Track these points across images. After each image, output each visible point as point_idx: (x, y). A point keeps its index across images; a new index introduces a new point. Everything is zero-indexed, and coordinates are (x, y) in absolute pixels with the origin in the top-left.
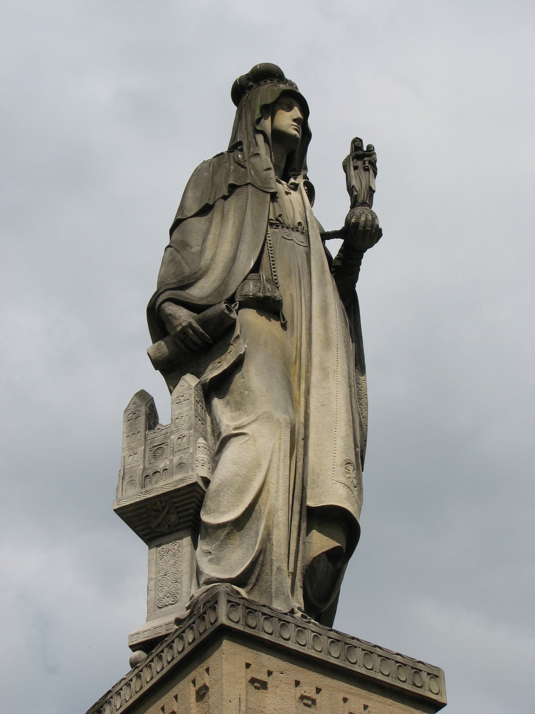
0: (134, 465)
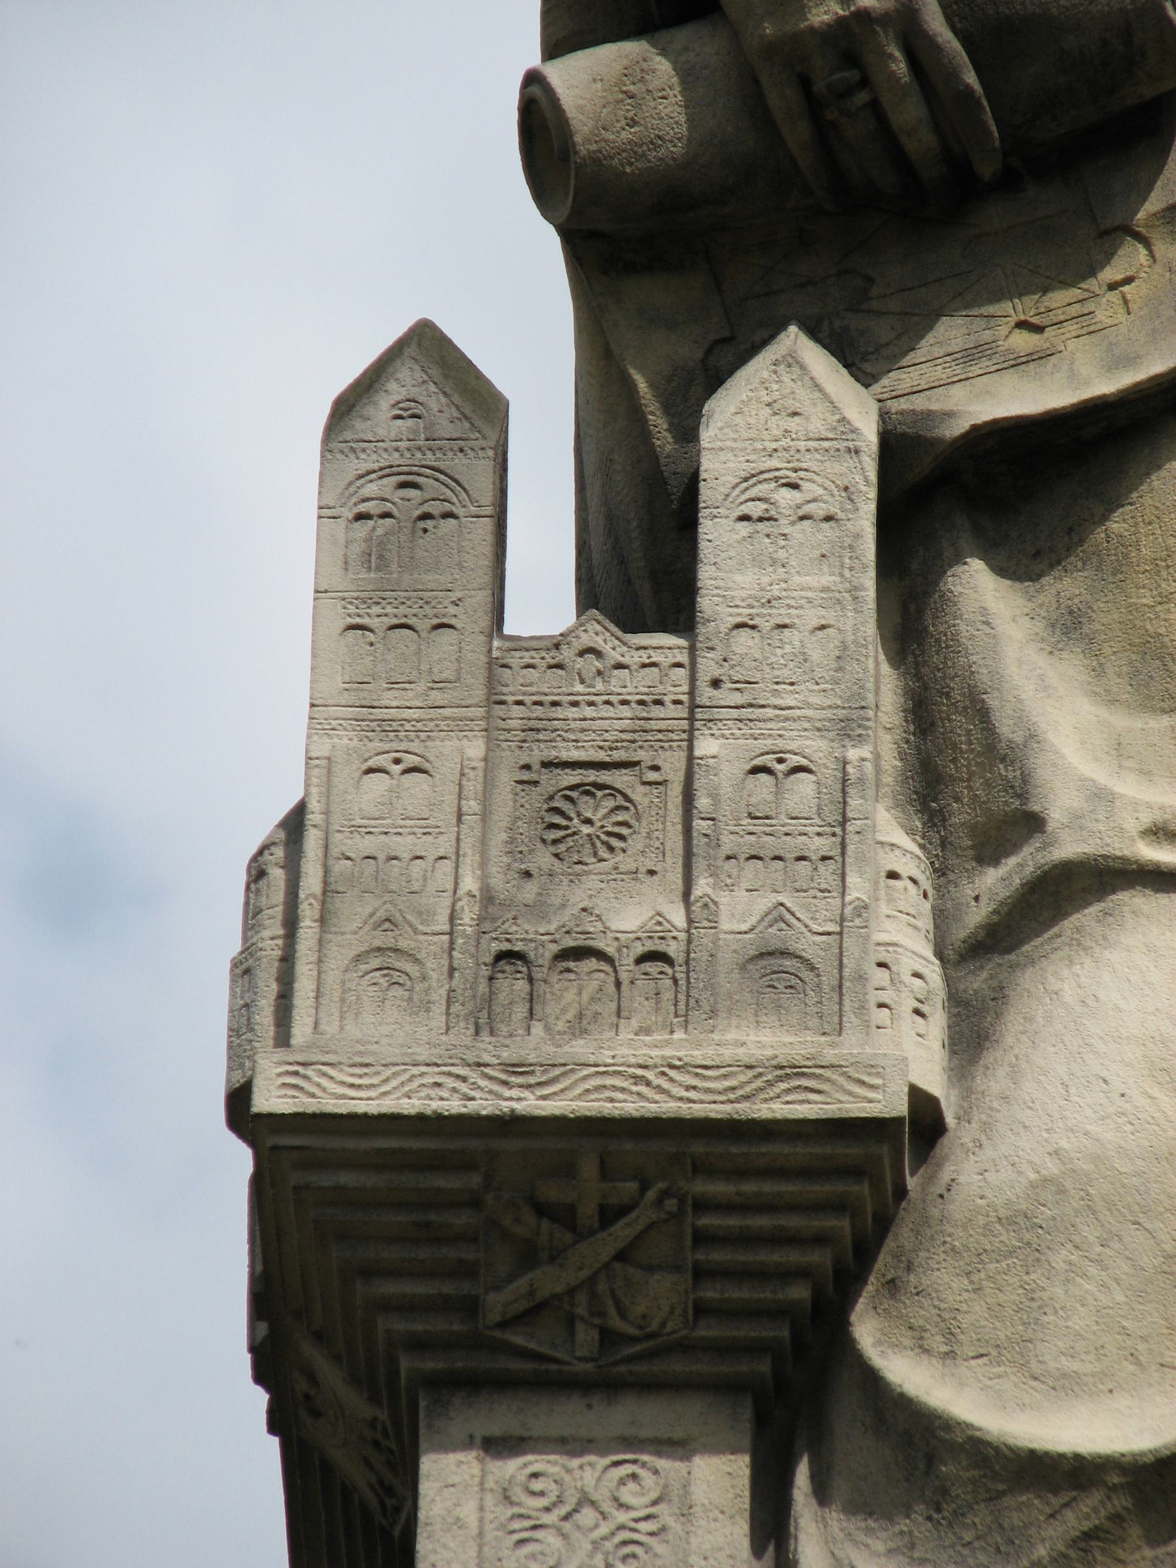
0: (404, 845)
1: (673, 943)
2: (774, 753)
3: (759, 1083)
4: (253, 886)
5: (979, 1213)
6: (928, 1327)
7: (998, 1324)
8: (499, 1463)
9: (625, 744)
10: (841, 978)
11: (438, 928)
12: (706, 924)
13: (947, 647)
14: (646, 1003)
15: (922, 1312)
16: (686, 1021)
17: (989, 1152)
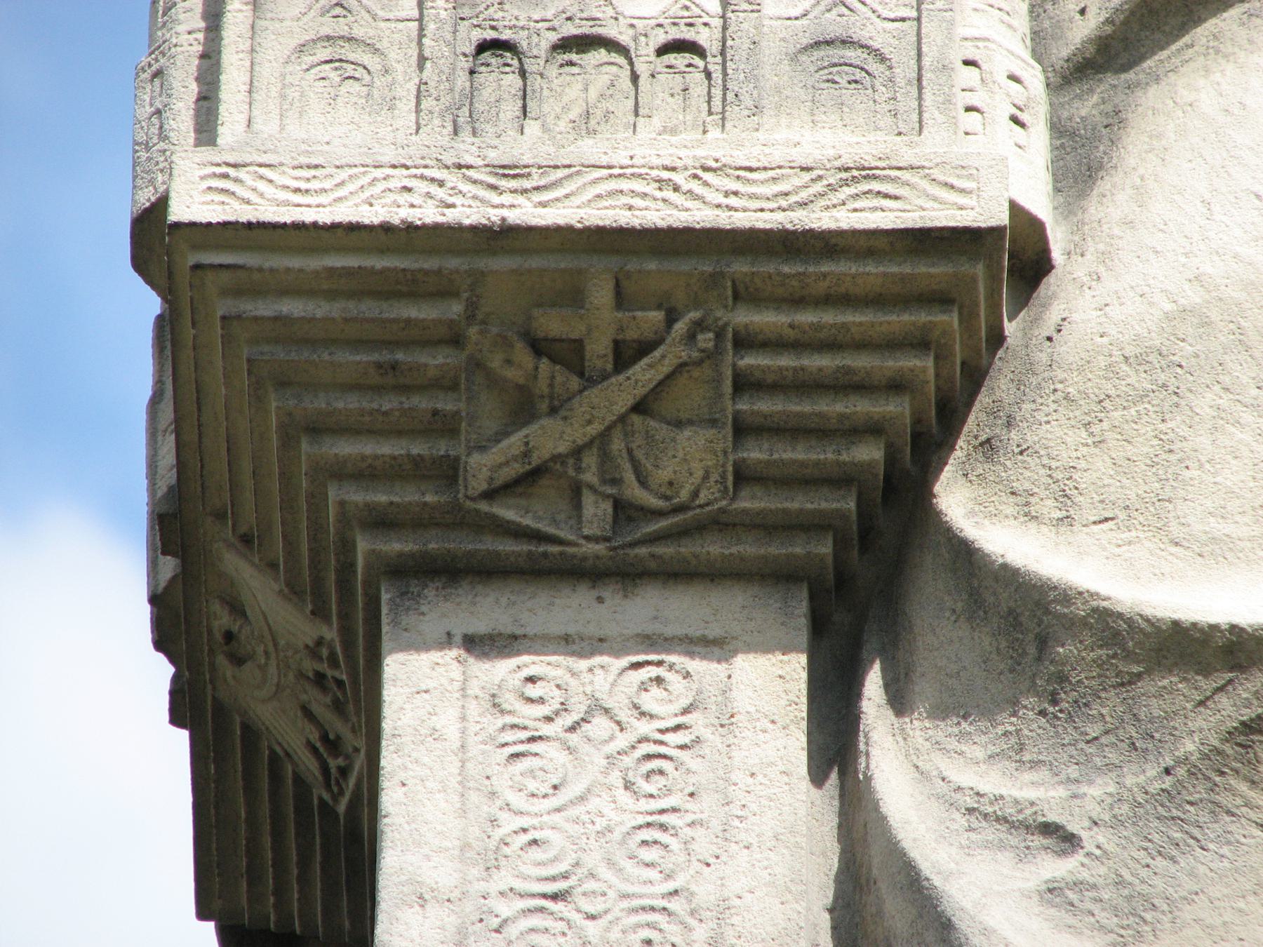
1: (705, 32)
3: (818, 187)
6: (1036, 490)
8: (486, 665)
10: (920, 69)
11: (403, 14)
12: (745, 6)
14: (670, 100)
16: (723, 119)
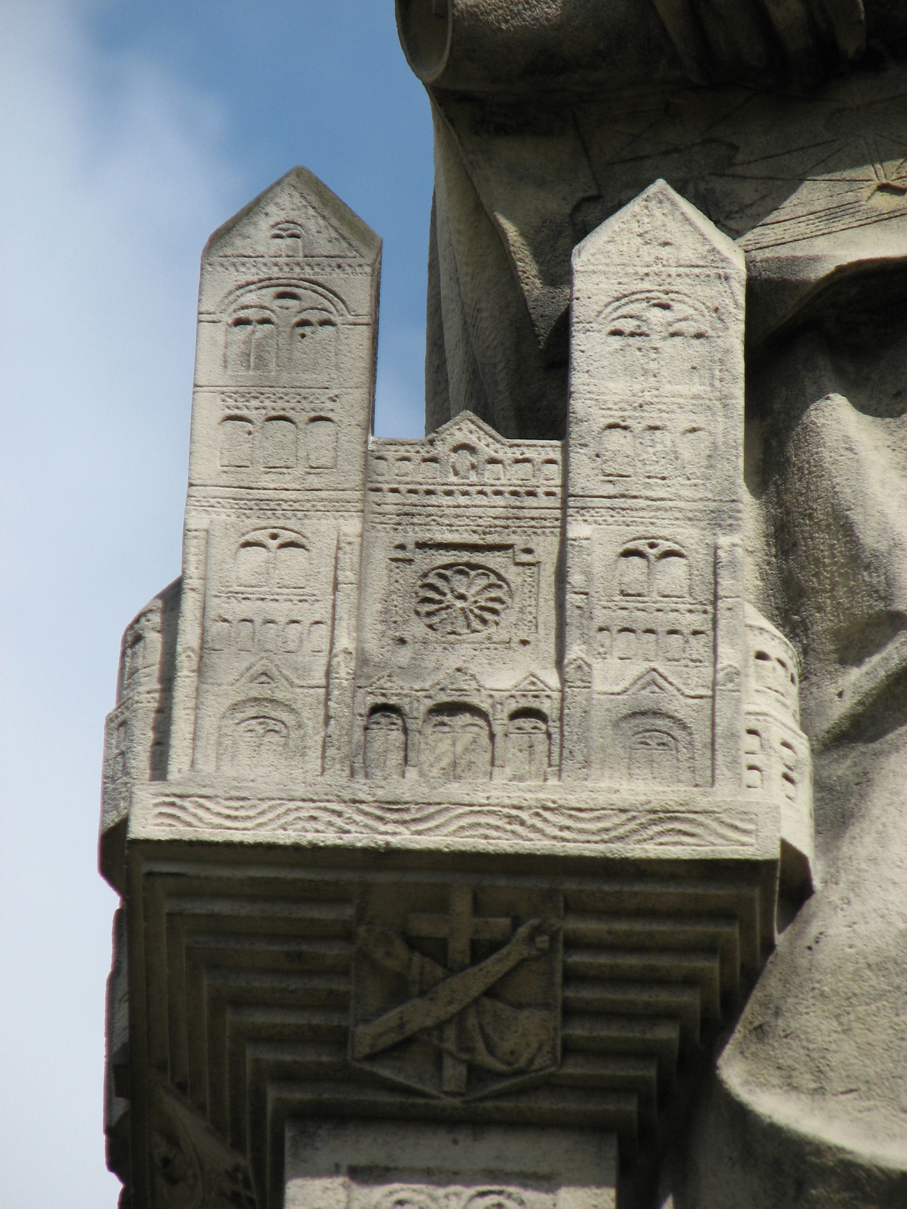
0: (281, 610)
1: (545, 700)
2: (646, 538)
3: (632, 825)
4: (129, 651)
5: (847, 960)
6: (797, 1066)
7: (867, 1062)
9: (498, 529)
10: (714, 735)
13: (810, 473)
14: (519, 754)
15: (790, 1053)
16: (560, 770)
17: (857, 906)
